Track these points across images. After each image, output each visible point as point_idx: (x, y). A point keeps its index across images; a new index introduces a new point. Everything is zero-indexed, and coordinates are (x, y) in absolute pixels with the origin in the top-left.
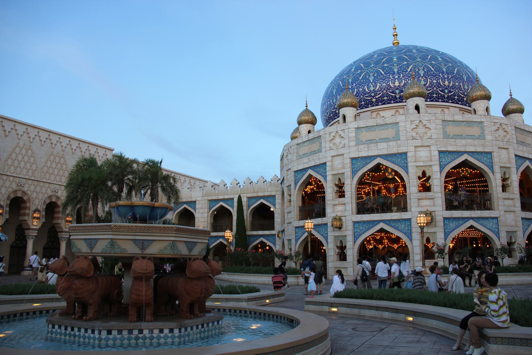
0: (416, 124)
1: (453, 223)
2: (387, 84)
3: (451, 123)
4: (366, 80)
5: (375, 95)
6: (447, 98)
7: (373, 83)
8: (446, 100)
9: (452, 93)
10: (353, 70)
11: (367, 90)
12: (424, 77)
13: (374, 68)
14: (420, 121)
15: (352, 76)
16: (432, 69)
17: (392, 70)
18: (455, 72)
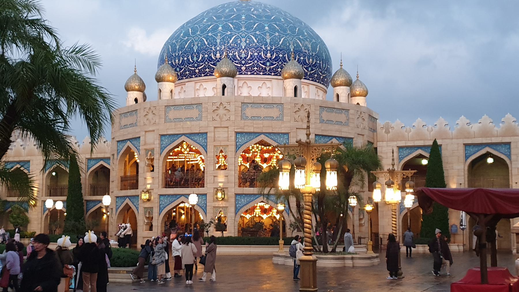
0: (217, 106)
1: (244, 199)
2: (209, 55)
3: (250, 105)
4: (190, 49)
5: (198, 66)
6: (269, 71)
7: (196, 53)
8: (268, 73)
9: (275, 66)
10: (205, 21)
11: (191, 60)
12: (245, 50)
13: (199, 37)
14: (221, 103)
15: (180, 42)
16: (255, 40)
17: (215, 40)
18: (281, 43)
